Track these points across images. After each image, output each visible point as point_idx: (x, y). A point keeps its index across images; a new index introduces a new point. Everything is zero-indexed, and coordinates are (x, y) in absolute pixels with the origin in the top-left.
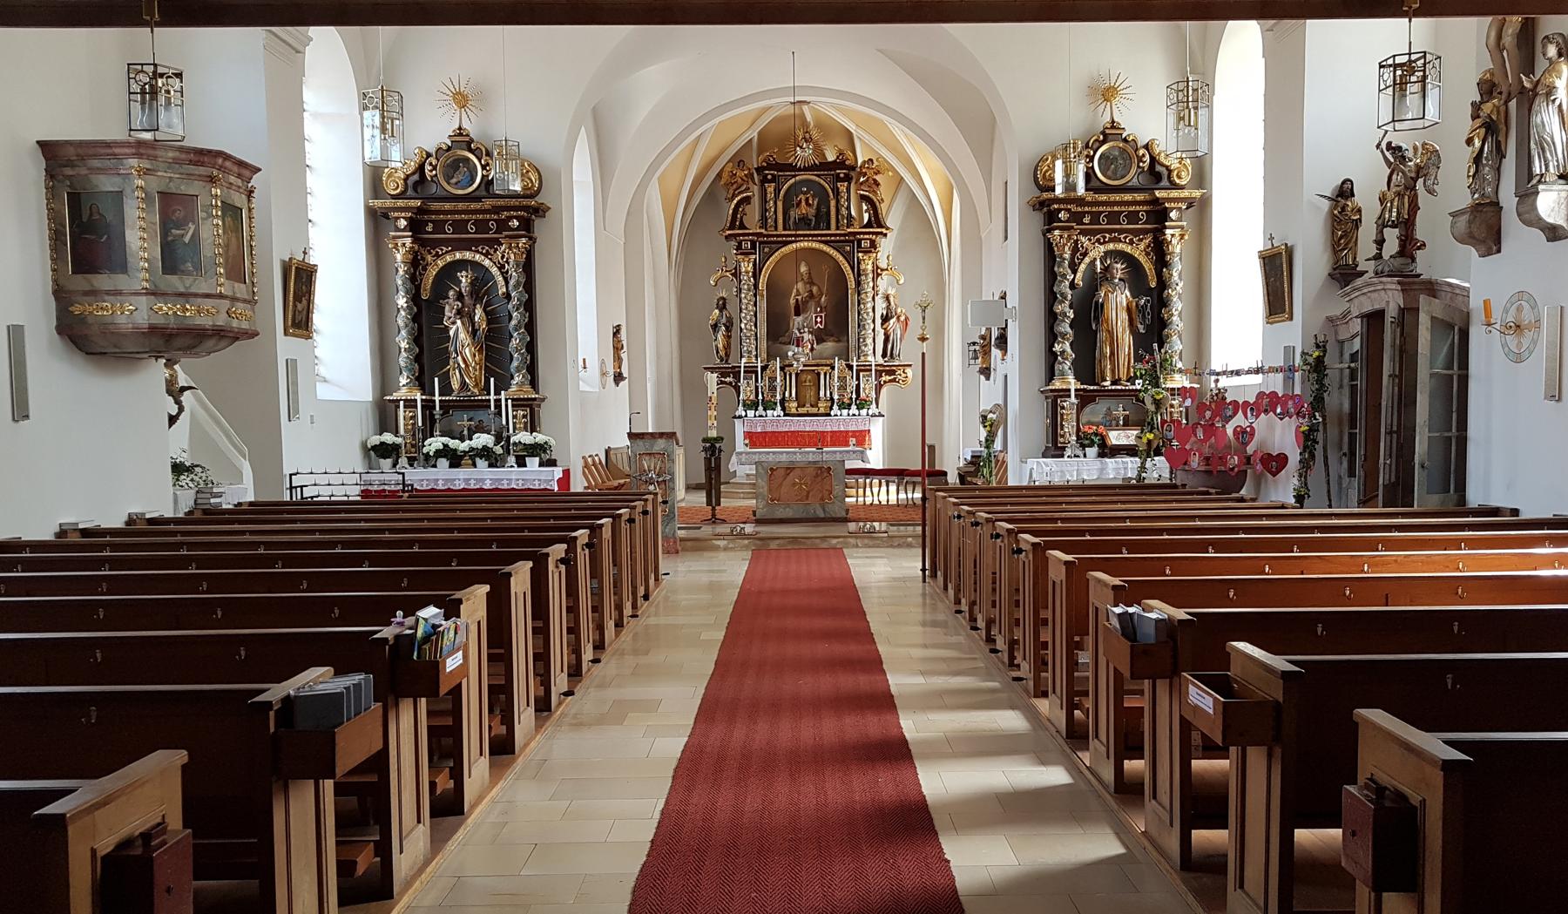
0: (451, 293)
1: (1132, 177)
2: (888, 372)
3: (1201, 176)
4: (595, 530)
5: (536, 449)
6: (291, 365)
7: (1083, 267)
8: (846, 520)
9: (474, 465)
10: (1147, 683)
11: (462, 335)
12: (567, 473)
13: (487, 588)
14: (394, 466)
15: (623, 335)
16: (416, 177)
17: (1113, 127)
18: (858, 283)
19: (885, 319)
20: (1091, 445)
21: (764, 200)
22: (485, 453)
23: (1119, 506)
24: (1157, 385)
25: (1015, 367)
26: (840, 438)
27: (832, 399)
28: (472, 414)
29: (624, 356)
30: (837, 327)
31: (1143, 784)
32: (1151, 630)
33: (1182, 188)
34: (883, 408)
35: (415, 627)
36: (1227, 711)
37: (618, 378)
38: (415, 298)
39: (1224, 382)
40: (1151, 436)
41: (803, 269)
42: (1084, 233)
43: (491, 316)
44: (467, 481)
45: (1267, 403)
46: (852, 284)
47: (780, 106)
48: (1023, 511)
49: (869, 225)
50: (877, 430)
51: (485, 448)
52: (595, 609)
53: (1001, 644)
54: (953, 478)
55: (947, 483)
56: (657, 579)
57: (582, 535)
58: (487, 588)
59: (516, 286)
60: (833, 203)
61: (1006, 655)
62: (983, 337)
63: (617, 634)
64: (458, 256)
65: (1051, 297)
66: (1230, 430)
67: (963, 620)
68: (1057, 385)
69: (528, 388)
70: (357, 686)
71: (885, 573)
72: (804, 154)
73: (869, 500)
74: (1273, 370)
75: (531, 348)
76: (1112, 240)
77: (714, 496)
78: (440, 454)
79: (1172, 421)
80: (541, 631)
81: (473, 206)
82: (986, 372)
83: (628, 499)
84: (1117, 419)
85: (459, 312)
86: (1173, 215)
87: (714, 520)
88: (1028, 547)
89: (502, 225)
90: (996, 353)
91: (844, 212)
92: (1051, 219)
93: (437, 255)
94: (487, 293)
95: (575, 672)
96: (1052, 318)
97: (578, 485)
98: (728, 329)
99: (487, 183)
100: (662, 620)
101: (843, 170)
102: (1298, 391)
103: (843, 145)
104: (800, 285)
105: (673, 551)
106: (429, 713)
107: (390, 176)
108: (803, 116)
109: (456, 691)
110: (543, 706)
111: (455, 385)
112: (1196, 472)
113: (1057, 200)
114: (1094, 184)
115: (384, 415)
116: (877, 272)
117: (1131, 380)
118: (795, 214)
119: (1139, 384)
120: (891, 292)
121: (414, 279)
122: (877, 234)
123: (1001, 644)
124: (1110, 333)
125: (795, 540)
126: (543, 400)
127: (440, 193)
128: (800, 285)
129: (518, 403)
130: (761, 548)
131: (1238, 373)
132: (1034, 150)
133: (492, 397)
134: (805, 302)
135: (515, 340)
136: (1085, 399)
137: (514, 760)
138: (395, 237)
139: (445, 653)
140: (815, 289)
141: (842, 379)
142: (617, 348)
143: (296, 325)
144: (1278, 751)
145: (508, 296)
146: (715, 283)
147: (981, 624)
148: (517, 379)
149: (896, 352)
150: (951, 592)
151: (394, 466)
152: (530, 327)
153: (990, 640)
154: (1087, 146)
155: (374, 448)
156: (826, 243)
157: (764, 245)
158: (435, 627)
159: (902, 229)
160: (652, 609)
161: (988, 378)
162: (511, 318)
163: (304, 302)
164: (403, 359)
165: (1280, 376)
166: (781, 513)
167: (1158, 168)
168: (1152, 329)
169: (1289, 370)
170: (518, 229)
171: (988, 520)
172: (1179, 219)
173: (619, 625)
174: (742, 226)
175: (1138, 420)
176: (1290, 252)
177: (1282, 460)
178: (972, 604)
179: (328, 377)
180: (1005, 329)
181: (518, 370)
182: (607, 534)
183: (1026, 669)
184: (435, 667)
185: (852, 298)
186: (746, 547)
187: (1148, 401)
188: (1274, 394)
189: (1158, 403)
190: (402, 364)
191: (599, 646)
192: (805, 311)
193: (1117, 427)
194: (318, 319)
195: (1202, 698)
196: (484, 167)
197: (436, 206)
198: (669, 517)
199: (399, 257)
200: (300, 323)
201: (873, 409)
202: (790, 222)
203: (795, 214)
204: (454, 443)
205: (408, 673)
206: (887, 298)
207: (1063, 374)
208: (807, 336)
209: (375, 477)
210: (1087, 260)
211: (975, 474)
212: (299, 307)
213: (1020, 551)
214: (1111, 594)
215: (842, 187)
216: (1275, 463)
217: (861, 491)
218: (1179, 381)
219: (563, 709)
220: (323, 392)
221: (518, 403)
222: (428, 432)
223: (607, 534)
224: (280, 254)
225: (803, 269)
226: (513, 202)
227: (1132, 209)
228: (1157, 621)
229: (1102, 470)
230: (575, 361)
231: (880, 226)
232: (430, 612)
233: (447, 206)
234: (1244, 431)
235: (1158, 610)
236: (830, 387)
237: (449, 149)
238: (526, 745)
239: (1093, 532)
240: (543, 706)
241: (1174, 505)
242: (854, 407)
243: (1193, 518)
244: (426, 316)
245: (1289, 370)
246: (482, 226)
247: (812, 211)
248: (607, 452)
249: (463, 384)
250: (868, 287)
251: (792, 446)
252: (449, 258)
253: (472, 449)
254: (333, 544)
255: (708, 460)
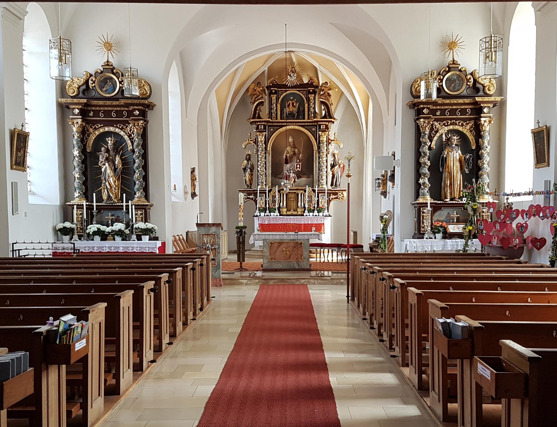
0: (103, 149)
1: (463, 90)
2: (334, 194)
3: (501, 90)
4: (172, 274)
5: (147, 231)
6: (14, 185)
7: (436, 138)
8: (309, 270)
9: (114, 239)
10: (458, 362)
11: (109, 171)
12: (164, 244)
13: (105, 304)
14: (71, 239)
15: (196, 173)
16: (84, 87)
17: (454, 63)
18: (319, 148)
19: (333, 166)
20: (439, 232)
21: (271, 104)
22: (120, 233)
23: (452, 265)
24: (474, 201)
25: (399, 191)
26: (308, 227)
27: (305, 207)
28: (113, 212)
29: (197, 184)
30: (308, 170)
31: (457, 417)
32: (459, 332)
33: (491, 96)
34: (331, 211)
35: (58, 326)
36: (497, 378)
37: (194, 195)
38: (83, 151)
39: (511, 199)
40: (471, 228)
41: (291, 140)
42: (436, 120)
43: (124, 161)
44: (110, 247)
45: (535, 211)
46: (315, 148)
47: (279, 53)
48: (397, 266)
49: (325, 117)
50: (328, 223)
51: (120, 230)
52: (171, 316)
53: (385, 337)
54: (366, 249)
55: (363, 251)
56: (208, 300)
57: (165, 277)
58: (105, 304)
59: (137, 146)
60: (306, 105)
61: (388, 343)
62: (383, 176)
63: (184, 329)
64: (107, 129)
65: (418, 154)
66: (514, 226)
67: (367, 324)
68: (421, 200)
69: (143, 199)
70: (19, 359)
71: (328, 298)
72: (292, 79)
73: (322, 260)
74: (537, 193)
75: (145, 178)
76: (451, 124)
77: (241, 258)
78: (95, 233)
79: (483, 220)
80: (138, 327)
81: (115, 103)
82: (384, 194)
83: (191, 256)
84: (453, 219)
85: (107, 159)
86: (485, 110)
87: (241, 269)
88: (399, 285)
89: (130, 113)
90: (389, 184)
91: (312, 110)
92: (419, 113)
93: (95, 129)
94: (122, 149)
95: (158, 350)
96: (418, 165)
97: (170, 250)
98: (252, 170)
99: (122, 91)
100: (211, 322)
101: (312, 88)
102: (552, 204)
103: (312, 75)
104: (288, 148)
105: (218, 285)
106: (68, 373)
107: (70, 86)
108: (291, 59)
109: (84, 360)
110: (138, 368)
111: (105, 197)
112: (495, 247)
113: (422, 103)
114: (443, 94)
115: (66, 212)
116: (329, 142)
117: (461, 198)
118: (287, 110)
119: (464, 201)
120: (336, 152)
121: (83, 141)
122: (329, 122)
123: (385, 337)
124: (450, 173)
125: (282, 280)
126: (152, 206)
127: (97, 96)
128: (288, 148)
129: (138, 207)
130: (264, 283)
131: (519, 195)
132: (410, 76)
133: (124, 204)
134: (291, 157)
135: (136, 175)
136: (436, 208)
137: (119, 398)
138: (72, 119)
139: (75, 340)
140: (296, 150)
141: (310, 197)
142: (193, 180)
143: (17, 164)
144: (527, 402)
145: (133, 151)
146: (245, 147)
147: (376, 326)
148: (138, 195)
149: (338, 183)
150: (361, 308)
151: (71, 239)
152: (145, 167)
153: (380, 335)
154: (439, 74)
155: (60, 230)
156: (302, 126)
157: (270, 127)
158: (70, 325)
159: (342, 120)
160: (205, 316)
161: (385, 197)
162: (134, 162)
163: (22, 152)
164: (76, 184)
165: (542, 196)
166: (275, 266)
167: (478, 85)
168: (473, 171)
169: (547, 193)
170: (138, 115)
171: (379, 271)
172: (489, 113)
173: (185, 324)
174: (259, 117)
175: (464, 220)
176: (548, 130)
177: (543, 242)
178: (371, 315)
179: (35, 192)
180: (394, 171)
181: (138, 190)
182: (179, 276)
183: (397, 351)
184: (68, 348)
185: (316, 155)
186: (257, 283)
187: (469, 209)
188: (539, 206)
189: (475, 210)
190: (76, 186)
191: (173, 335)
192: (291, 162)
193: (453, 223)
194: (29, 161)
195: (485, 371)
196: (120, 83)
197: (95, 102)
198: (217, 268)
199: (75, 129)
200: (20, 163)
201: (326, 213)
202: (284, 113)
203: (287, 110)
204: (103, 228)
205: (52, 351)
206: (334, 155)
207: (424, 195)
208: (292, 175)
209: (59, 245)
210: (438, 135)
211: (376, 247)
212: (19, 154)
213: (394, 287)
214: (440, 312)
215: (311, 97)
216: (540, 243)
217: (318, 255)
218: (487, 199)
219: (149, 370)
220: (32, 200)
221: (138, 207)
222: (90, 221)
223: (179, 276)
224: (9, 126)
225: (291, 140)
226: (136, 101)
227: (463, 107)
228: (463, 327)
229: (444, 246)
230: (169, 186)
231: (331, 117)
232: (69, 317)
233: (101, 103)
234: (522, 226)
235: (464, 321)
236: (304, 201)
237: (102, 72)
238: (127, 390)
239: (435, 278)
240: (138, 368)
241: (482, 265)
242: (316, 211)
243: (491, 272)
244: (89, 160)
245: (547, 193)
246: (119, 114)
247: (295, 110)
248: (187, 233)
249: (109, 197)
250: (324, 149)
251: (281, 231)
252: (101, 130)
253: (113, 231)
254: (29, 281)
255: (238, 238)
